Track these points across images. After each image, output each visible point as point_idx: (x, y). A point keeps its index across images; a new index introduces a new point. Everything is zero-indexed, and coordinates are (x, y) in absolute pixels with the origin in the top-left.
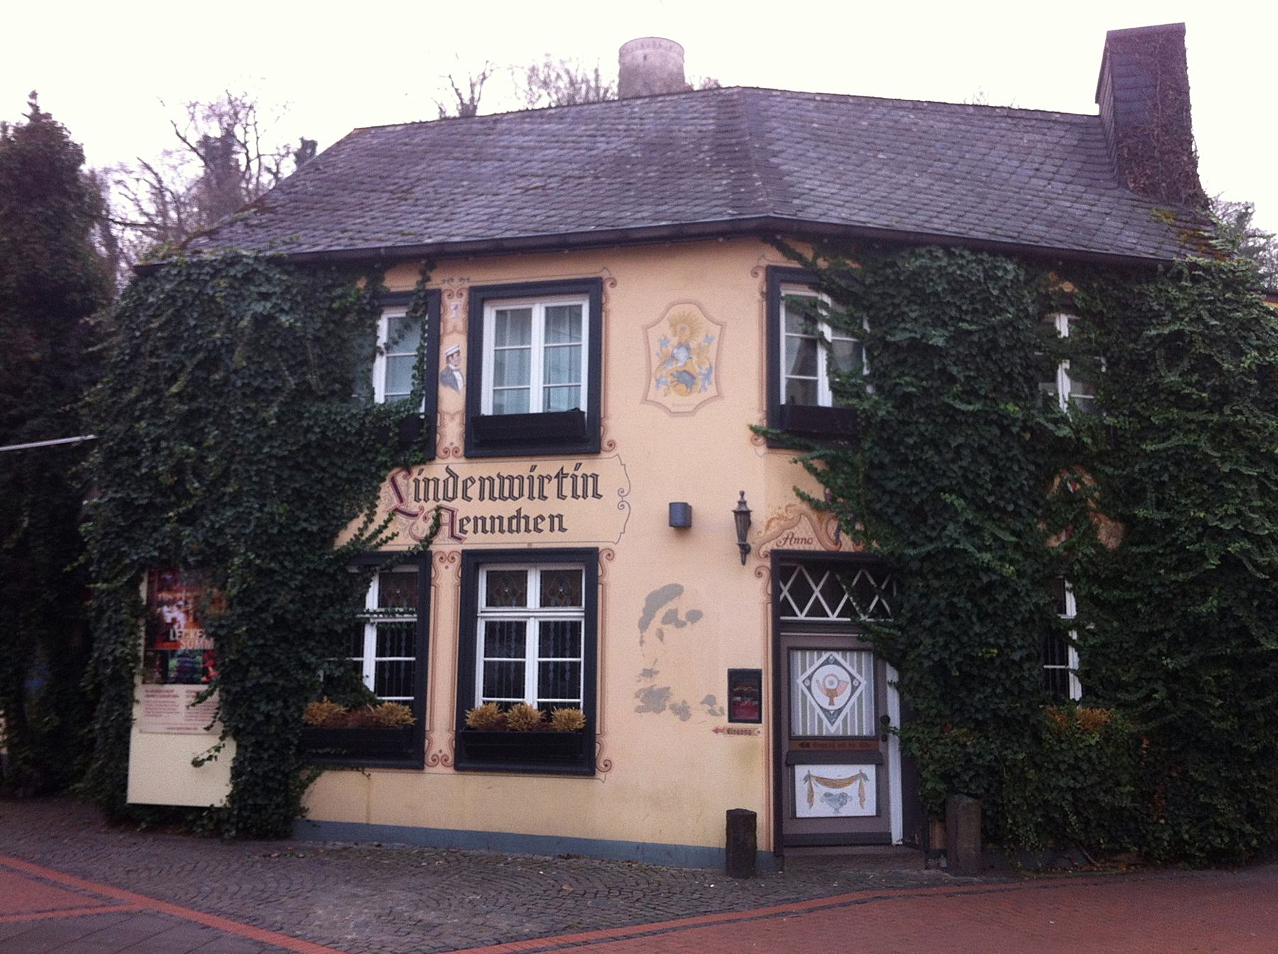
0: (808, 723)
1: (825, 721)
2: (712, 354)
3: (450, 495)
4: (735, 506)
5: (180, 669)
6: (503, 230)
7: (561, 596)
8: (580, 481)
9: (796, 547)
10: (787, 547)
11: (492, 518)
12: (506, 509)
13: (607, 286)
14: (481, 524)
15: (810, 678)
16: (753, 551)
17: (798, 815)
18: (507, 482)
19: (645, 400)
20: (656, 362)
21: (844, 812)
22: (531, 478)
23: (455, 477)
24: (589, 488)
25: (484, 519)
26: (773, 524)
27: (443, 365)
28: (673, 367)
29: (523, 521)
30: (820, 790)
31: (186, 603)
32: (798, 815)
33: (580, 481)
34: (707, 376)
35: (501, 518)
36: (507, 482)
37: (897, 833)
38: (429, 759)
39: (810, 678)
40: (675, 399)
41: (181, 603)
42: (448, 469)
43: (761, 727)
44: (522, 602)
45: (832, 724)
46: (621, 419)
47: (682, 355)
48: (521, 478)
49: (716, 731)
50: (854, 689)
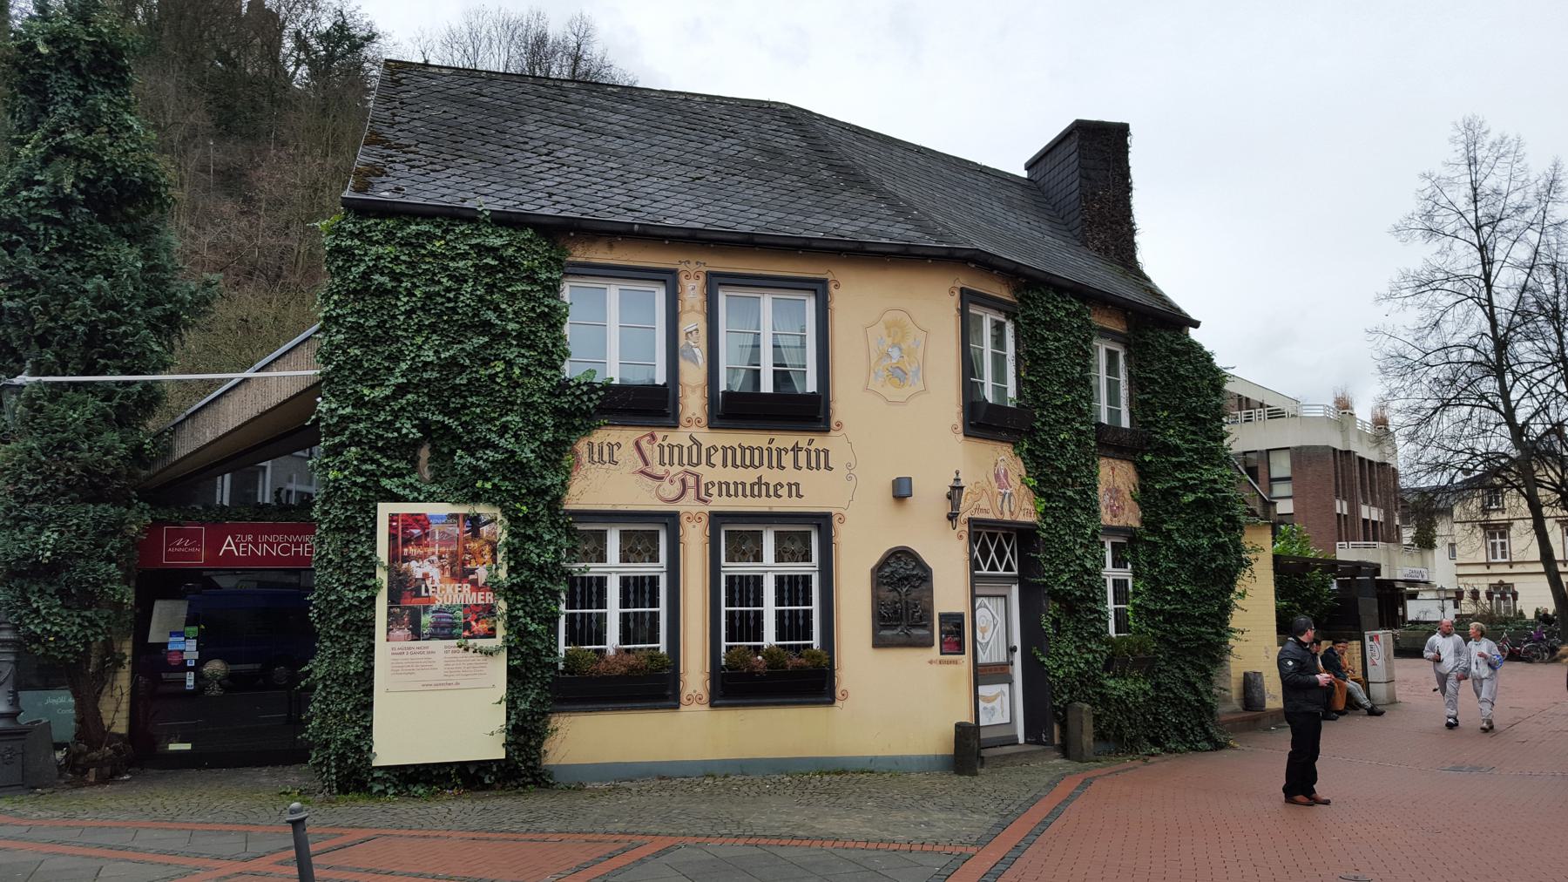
4: (951, 483)
5: (435, 626)
6: (787, 230)
7: (639, 554)
8: (813, 455)
10: (976, 516)
11: (736, 484)
12: (749, 476)
13: (832, 287)
14: (725, 488)
22: (769, 450)
23: (699, 445)
24: (822, 461)
25: (728, 484)
28: (887, 363)
31: (440, 558)
35: (744, 484)
38: (683, 698)
40: (891, 391)
41: (435, 558)
42: (691, 437)
44: (758, 557)
46: (841, 407)
47: (895, 353)
48: (761, 449)
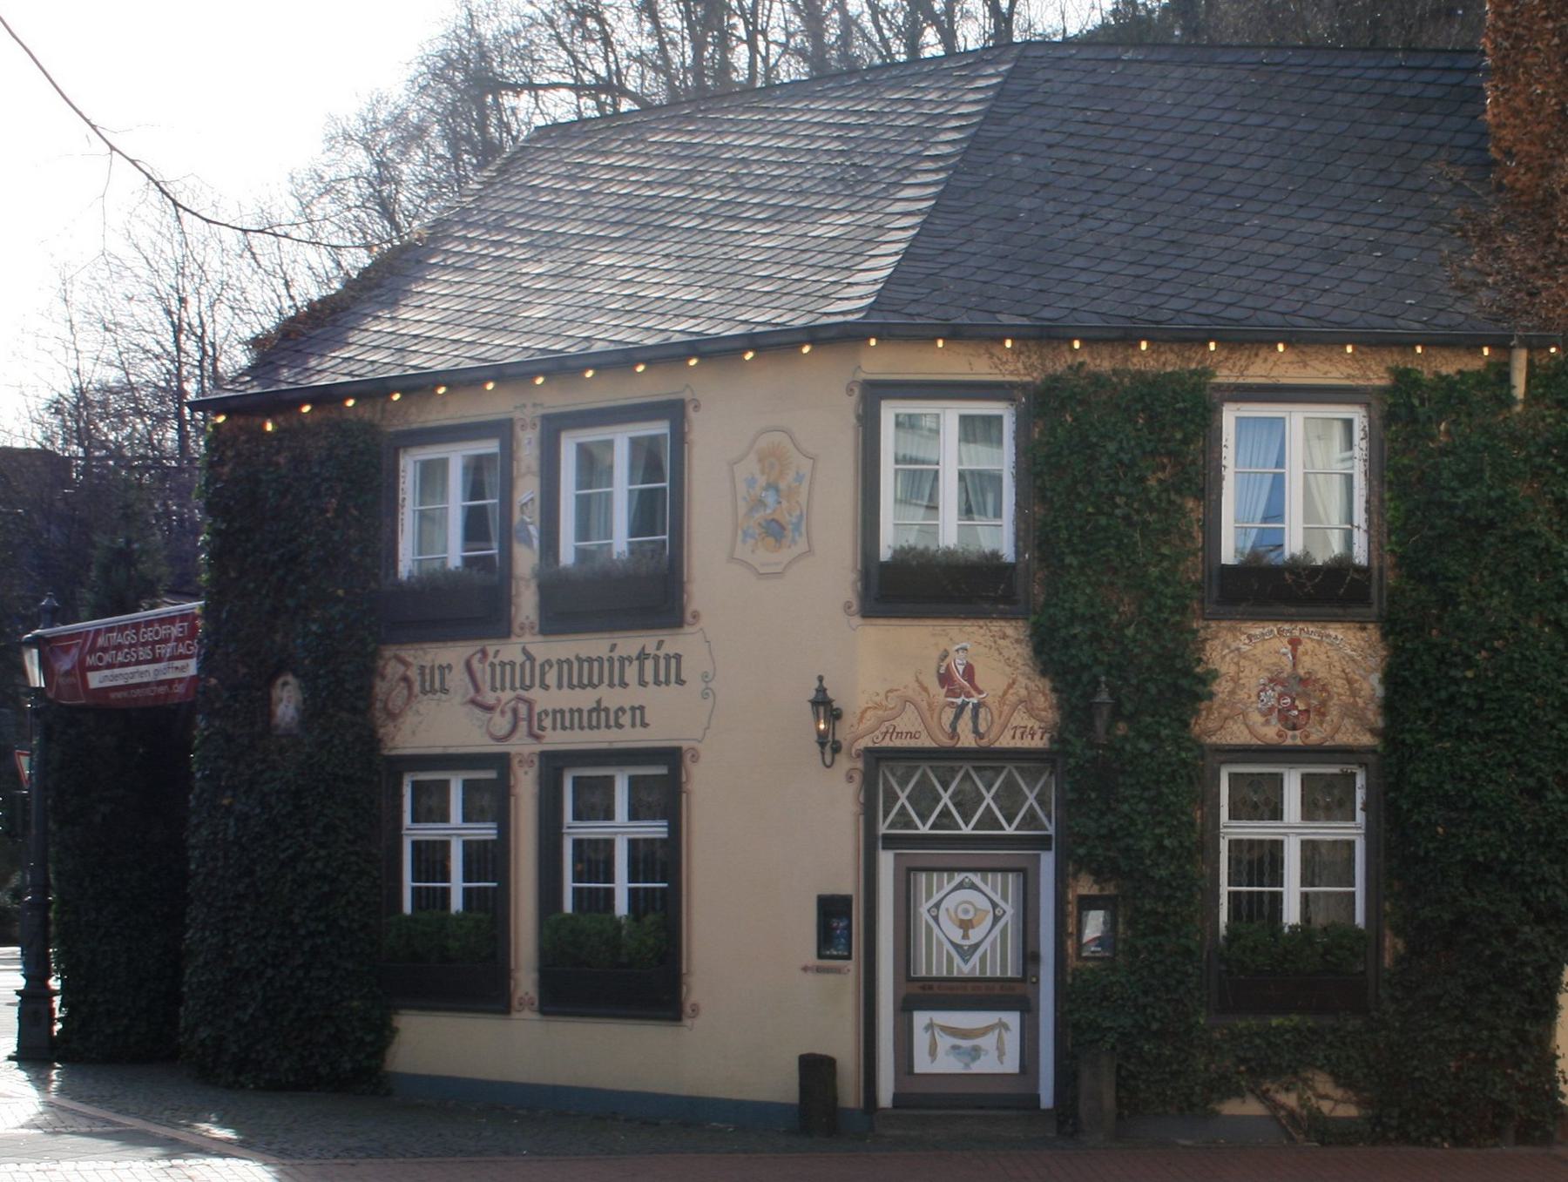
0: (935, 962)
1: (957, 959)
2: (803, 499)
3: (528, 682)
4: (812, 694)
8: (662, 663)
9: (898, 743)
11: (571, 711)
12: (584, 699)
15: (937, 905)
16: (844, 750)
17: (917, 1070)
18: (586, 665)
19: (732, 559)
20: (742, 508)
21: (977, 1068)
24: (671, 672)
26: (869, 714)
27: (517, 517)
28: (760, 515)
29: (603, 715)
30: (945, 1042)
32: (917, 1070)
33: (662, 663)
34: (797, 527)
36: (586, 665)
37: (1047, 1099)
38: (515, 1003)
39: (937, 905)
43: (851, 965)
45: (966, 962)
47: (770, 498)
48: (600, 659)
49: (805, 969)
50: (996, 919)
